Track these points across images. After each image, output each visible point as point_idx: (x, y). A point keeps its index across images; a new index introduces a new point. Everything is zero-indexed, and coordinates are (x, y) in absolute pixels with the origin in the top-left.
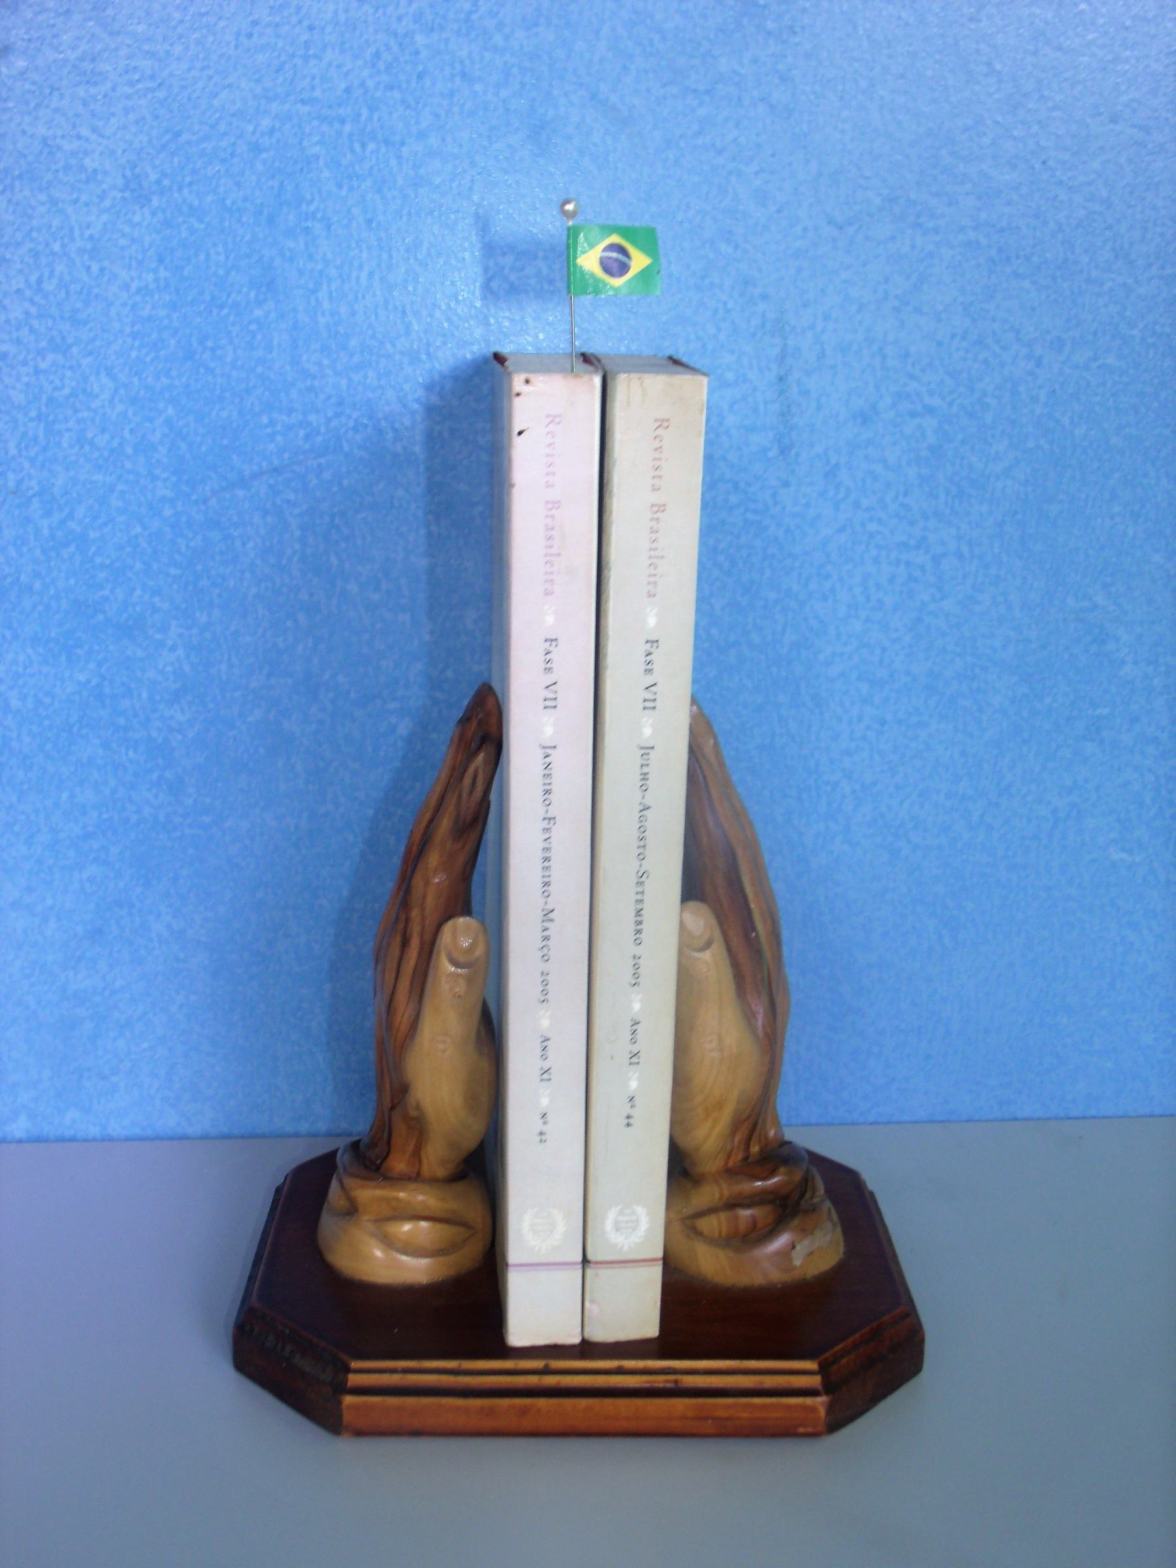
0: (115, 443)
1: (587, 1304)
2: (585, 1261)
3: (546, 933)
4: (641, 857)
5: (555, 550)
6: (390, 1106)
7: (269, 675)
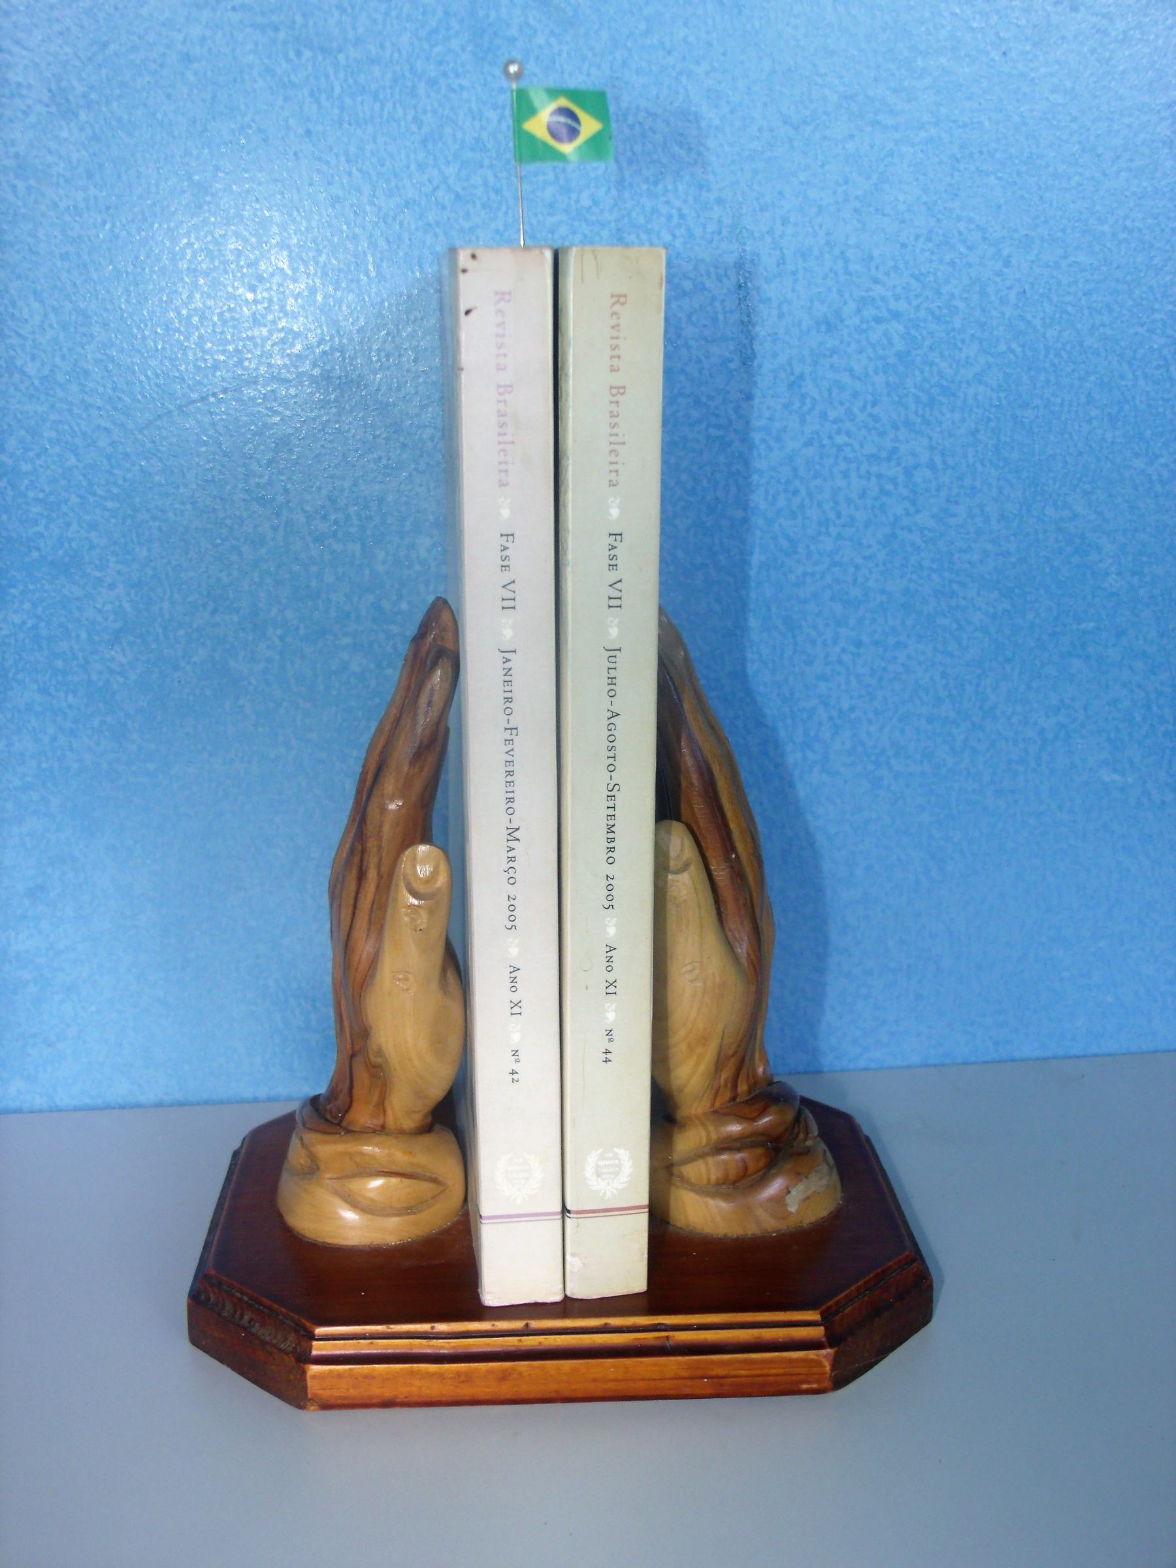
0: (46, 372)
1: (568, 1257)
2: (565, 1210)
3: (511, 854)
4: (611, 768)
5: (508, 438)
6: (350, 1053)
7: (214, 612)
